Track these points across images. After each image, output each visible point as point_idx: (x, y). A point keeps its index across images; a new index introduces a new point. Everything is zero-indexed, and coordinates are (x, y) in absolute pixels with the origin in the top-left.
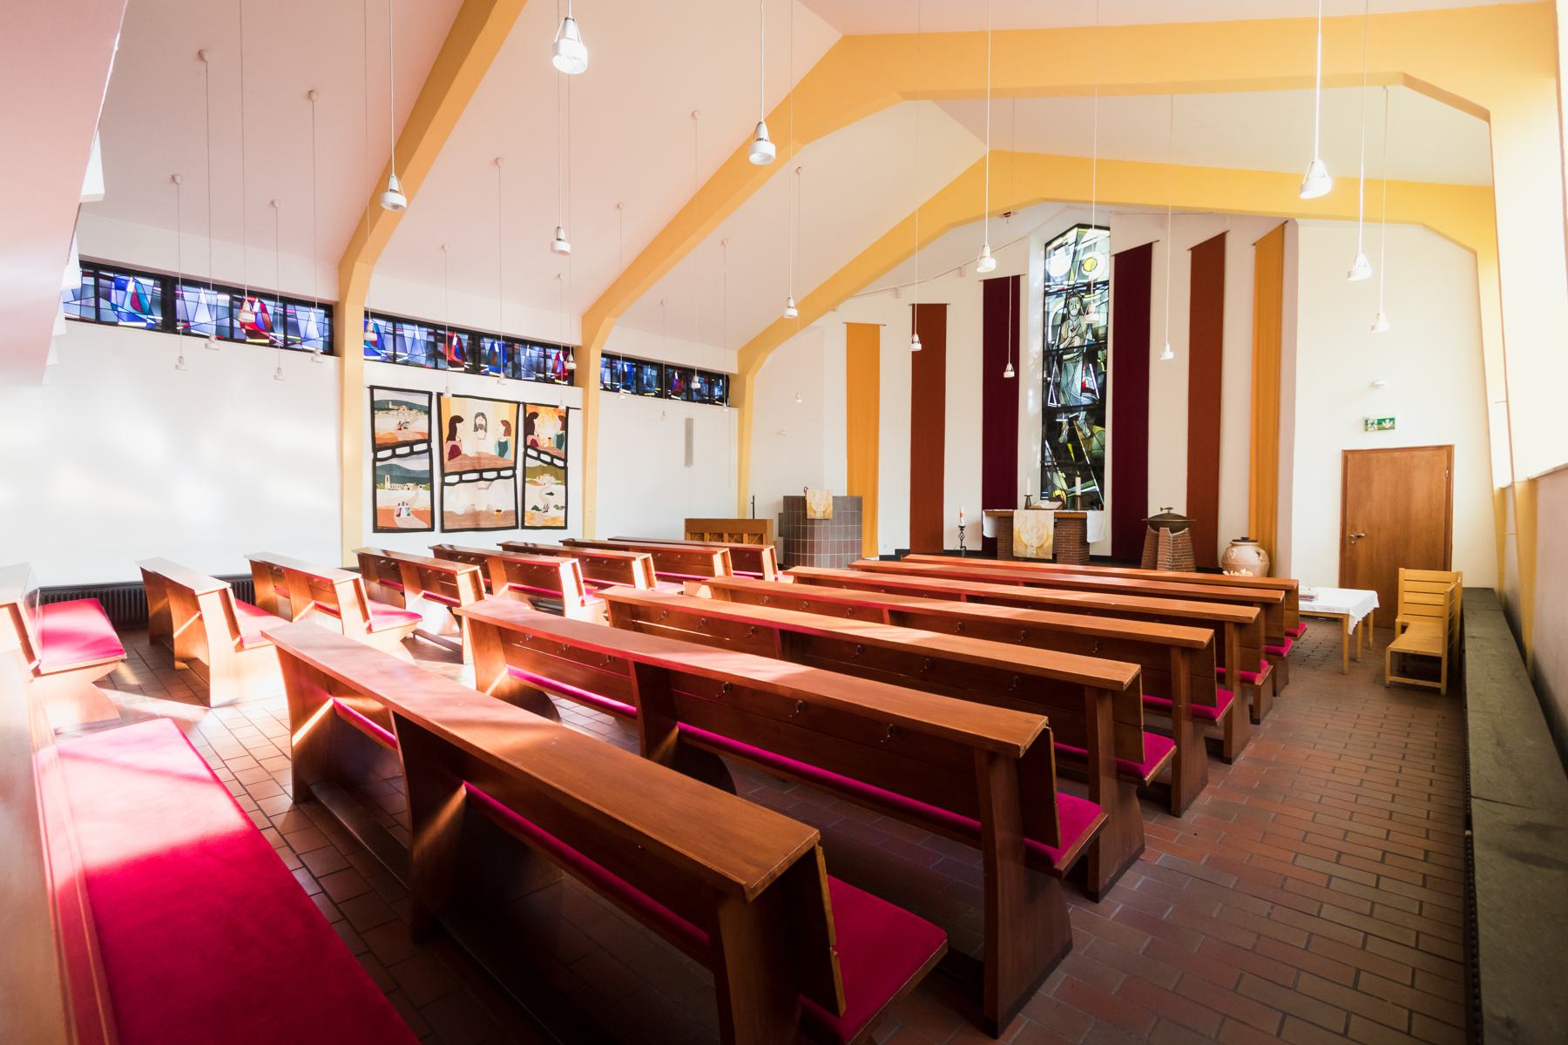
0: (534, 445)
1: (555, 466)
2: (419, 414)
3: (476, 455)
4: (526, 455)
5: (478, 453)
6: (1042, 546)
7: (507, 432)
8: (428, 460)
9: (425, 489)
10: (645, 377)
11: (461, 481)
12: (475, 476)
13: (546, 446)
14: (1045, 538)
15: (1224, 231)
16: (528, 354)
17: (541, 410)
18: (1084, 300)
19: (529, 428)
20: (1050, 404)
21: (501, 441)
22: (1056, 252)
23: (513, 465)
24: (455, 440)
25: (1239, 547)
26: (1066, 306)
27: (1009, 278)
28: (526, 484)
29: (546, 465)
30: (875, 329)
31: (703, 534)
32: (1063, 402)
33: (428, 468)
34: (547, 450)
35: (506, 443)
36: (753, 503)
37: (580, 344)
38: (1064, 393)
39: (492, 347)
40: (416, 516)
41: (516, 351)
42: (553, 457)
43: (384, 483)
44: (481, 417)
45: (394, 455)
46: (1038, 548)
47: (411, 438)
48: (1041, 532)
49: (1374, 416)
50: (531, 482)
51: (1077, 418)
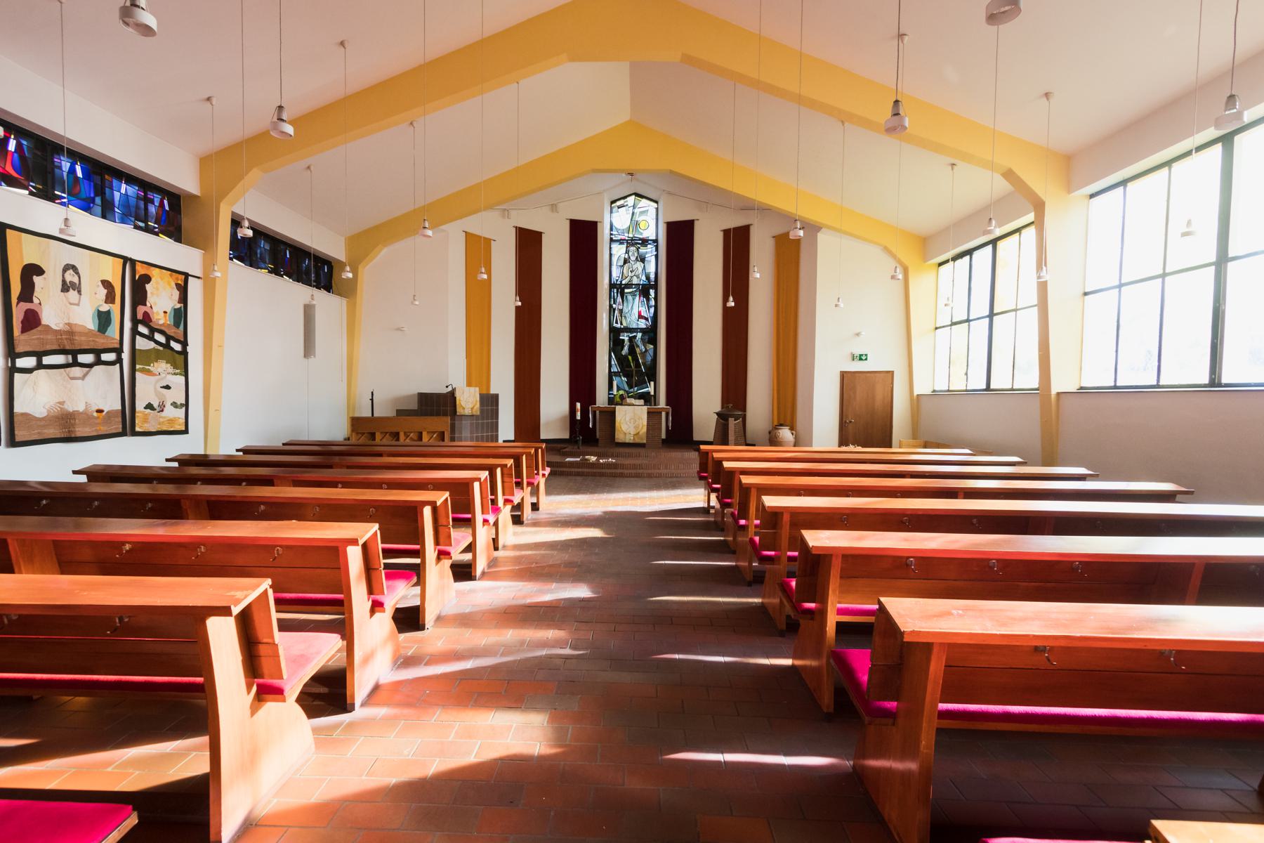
0: (147, 320)
1: (172, 349)
3: (67, 328)
4: (135, 332)
5: (69, 324)
7: (110, 298)
10: (259, 251)
11: (40, 366)
12: (59, 359)
13: (161, 322)
14: (640, 427)
15: (750, 223)
16: (123, 191)
17: (155, 273)
18: (640, 250)
19: (139, 295)
20: (615, 325)
21: (176, 307)
22: (620, 209)
23: (117, 346)
26: (627, 252)
28: (137, 373)
29: (161, 348)
30: (488, 242)
32: (625, 324)
34: (163, 328)
35: (108, 312)
36: (372, 400)
37: (199, 194)
39: (72, 171)
41: (107, 183)
42: (169, 338)
44: (71, 271)
49: (857, 352)
50: (142, 371)
51: (635, 337)
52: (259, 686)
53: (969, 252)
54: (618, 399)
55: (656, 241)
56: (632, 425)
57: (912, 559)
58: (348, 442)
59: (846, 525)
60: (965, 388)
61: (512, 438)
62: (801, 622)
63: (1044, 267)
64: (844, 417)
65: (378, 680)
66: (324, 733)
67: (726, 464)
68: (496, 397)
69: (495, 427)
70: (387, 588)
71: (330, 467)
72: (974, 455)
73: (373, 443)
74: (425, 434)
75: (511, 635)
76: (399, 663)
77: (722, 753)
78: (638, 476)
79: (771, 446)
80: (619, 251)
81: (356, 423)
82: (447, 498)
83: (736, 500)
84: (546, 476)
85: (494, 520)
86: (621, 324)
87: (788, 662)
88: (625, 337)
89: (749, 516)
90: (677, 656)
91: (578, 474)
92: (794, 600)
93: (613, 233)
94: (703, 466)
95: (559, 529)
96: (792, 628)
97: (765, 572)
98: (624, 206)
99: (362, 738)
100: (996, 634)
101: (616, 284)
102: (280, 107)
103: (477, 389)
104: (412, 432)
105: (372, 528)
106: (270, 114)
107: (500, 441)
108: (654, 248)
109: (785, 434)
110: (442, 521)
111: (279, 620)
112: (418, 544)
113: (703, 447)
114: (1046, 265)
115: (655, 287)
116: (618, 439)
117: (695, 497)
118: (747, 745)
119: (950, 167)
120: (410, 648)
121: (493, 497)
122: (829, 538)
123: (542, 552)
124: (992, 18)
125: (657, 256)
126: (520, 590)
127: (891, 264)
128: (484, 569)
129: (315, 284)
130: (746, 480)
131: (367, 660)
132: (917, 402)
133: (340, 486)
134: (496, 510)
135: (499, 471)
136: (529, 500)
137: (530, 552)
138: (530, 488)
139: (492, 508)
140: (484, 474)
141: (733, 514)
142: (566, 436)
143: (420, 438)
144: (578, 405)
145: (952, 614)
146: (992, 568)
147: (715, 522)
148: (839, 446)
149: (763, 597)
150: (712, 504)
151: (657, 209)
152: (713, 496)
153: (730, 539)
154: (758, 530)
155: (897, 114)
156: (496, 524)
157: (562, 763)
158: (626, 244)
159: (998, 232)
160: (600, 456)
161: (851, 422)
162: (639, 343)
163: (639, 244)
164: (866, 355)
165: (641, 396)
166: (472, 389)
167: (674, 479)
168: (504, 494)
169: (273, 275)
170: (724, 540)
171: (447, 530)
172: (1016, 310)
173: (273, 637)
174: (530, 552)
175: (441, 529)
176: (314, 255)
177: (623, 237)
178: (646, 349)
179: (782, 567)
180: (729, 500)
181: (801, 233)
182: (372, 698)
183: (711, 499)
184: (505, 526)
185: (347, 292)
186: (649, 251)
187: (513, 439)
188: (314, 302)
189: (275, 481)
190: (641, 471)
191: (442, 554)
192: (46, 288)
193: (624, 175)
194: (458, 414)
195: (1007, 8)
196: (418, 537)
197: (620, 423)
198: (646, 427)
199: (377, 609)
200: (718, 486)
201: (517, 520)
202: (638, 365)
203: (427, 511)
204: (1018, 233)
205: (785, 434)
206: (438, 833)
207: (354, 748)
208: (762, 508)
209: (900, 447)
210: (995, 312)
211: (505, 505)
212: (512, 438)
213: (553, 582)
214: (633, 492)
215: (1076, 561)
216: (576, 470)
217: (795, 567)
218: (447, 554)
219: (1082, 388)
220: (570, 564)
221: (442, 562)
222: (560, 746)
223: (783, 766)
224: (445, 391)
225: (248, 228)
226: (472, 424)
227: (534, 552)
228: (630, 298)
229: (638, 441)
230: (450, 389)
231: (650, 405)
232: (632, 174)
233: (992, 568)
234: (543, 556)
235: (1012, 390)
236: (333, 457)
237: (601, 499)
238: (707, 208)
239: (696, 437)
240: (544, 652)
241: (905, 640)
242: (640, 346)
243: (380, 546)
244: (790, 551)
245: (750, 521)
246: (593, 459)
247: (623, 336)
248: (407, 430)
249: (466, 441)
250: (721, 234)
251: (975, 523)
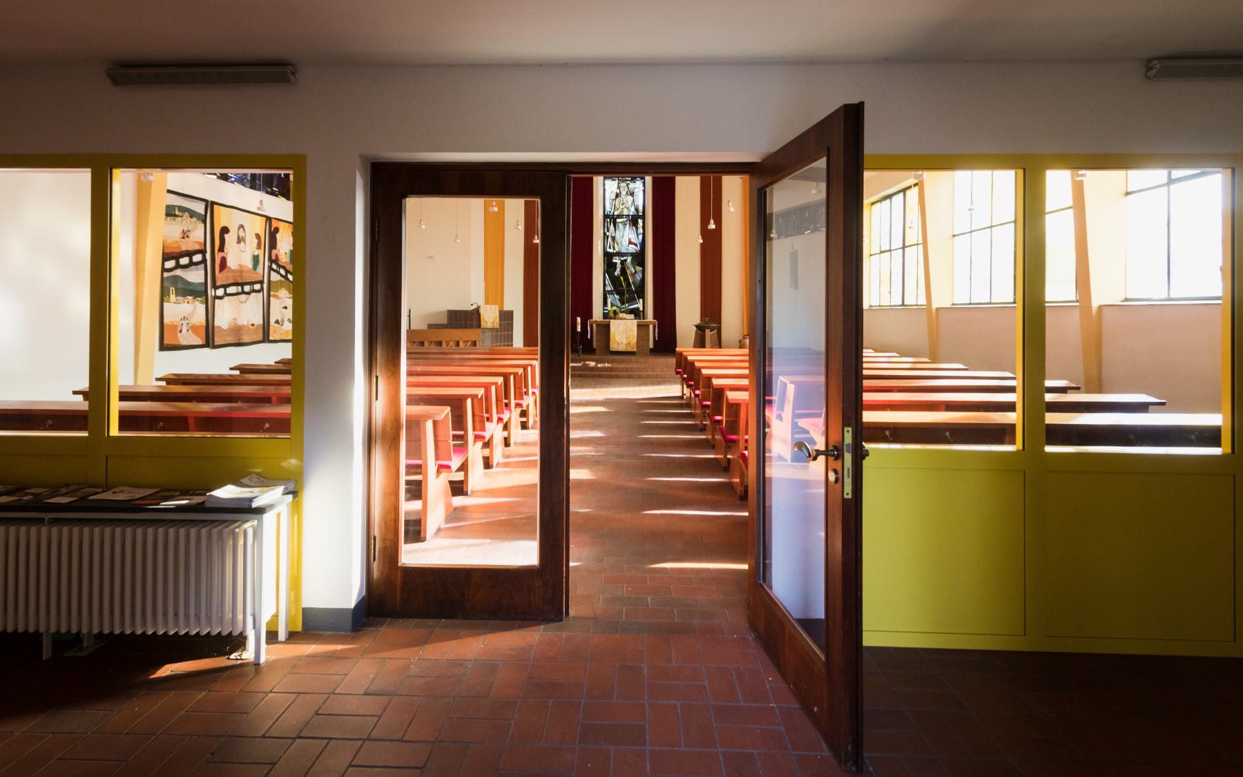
1: (288, 279)
2: (197, 222)
4: (270, 269)
5: (240, 266)
6: (629, 343)
7: (259, 247)
8: (203, 272)
9: (201, 302)
11: (226, 294)
13: (284, 261)
20: (608, 250)
24: (224, 251)
26: (619, 188)
28: (271, 298)
31: (423, 342)
33: (203, 281)
34: (284, 265)
35: (258, 256)
36: (409, 316)
38: (617, 243)
40: (193, 332)
42: (287, 272)
43: (169, 295)
45: (178, 266)
46: (626, 344)
47: (191, 247)
48: (628, 334)
51: (626, 260)
53: (889, 197)
69: (510, 338)
72: (932, 363)
74: (461, 343)
78: (629, 377)
86: (614, 249)
88: (617, 260)
89: (739, 432)
90: (653, 455)
94: (678, 365)
101: (610, 215)
103: (497, 307)
105: (446, 409)
108: (642, 184)
115: (643, 217)
117: (674, 390)
128: (440, 524)
140: (500, 380)
144: (579, 319)
160: (598, 361)
167: (660, 379)
168: (474, 429)
175: (441, 445)
190: (632, 373)
192: (230, 239)
201: (487, 464)
202: (629, 285)
203: (429, 425)
216: (579, 373)
223: (699, 482)
226: (492, 336)
228: (621, 226)
230: (474, 307)
231: (640, 319)
236: (281, 387)
240: (581, 454)
246: (592, 364)
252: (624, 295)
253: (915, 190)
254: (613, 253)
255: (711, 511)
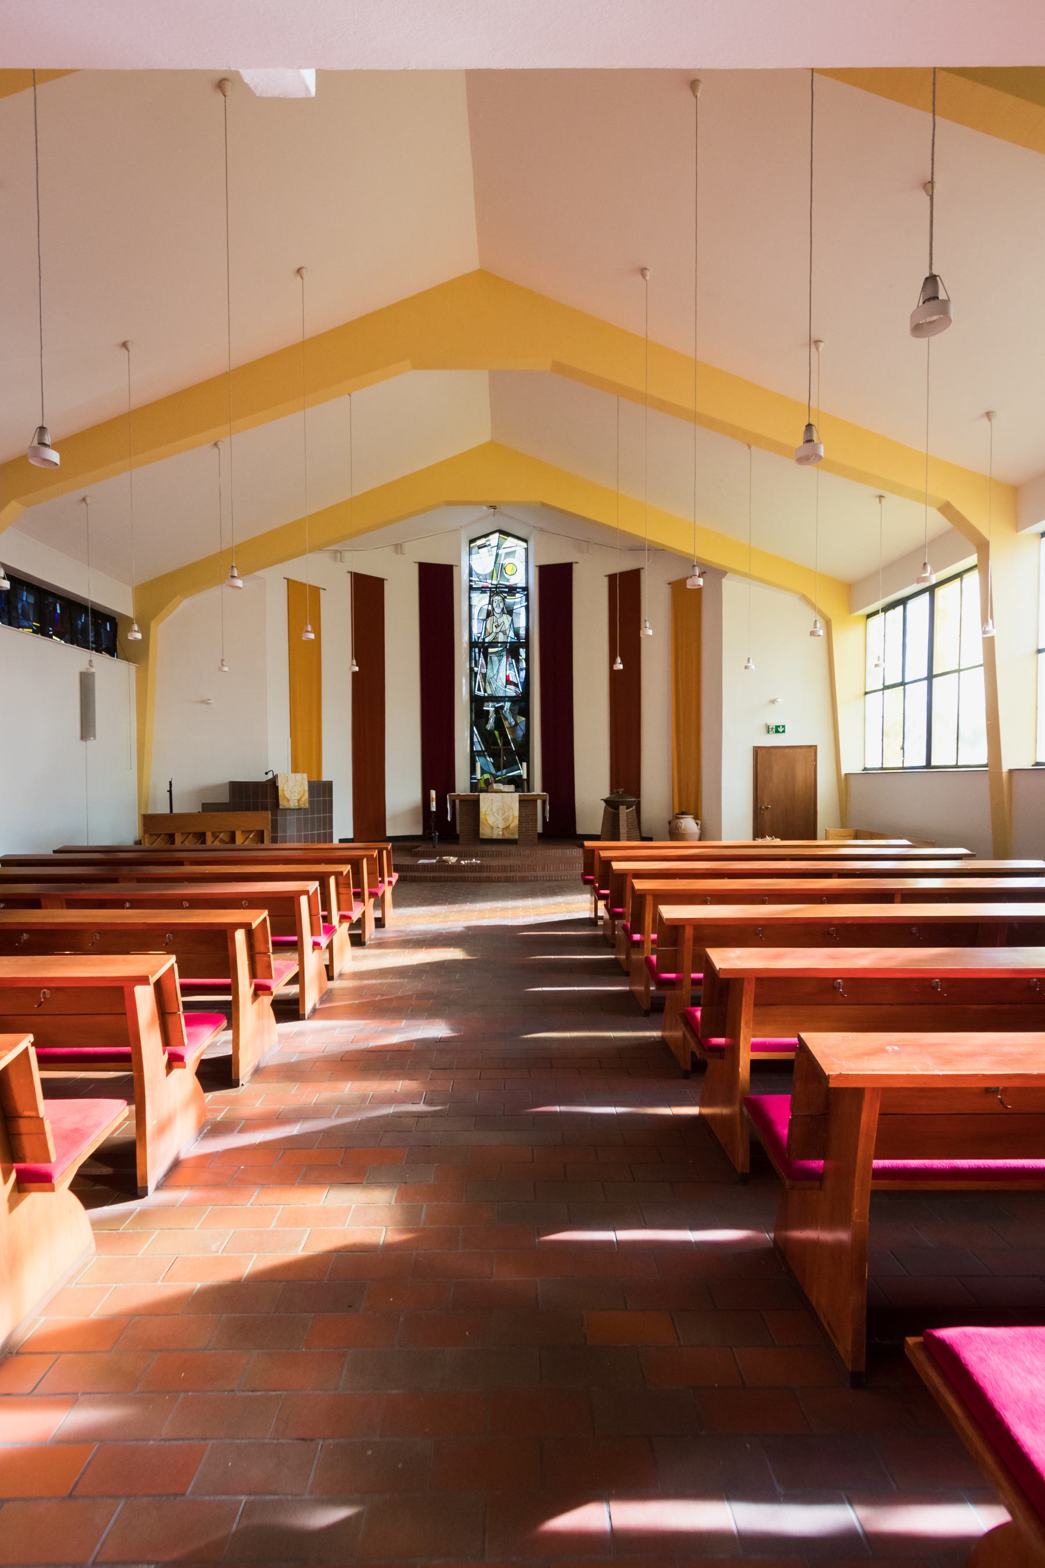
10: (20, 605)
14: (511, 820)
18: (506, 600)
20: (477, 693)
22: (480, 550)
25: (685, 819)
26: (491, 603)
27: (616, 574)
30: (316, 591)
36: (170, 791)
46: (503, 829)
49: (773, 723)
52: (19, 1172)
53: (903, 602)
54: (482, 785)
55: (526, 589)
56: (500, 817)
57: (840, 981)
58: (138, 847)
59: (761, 938)
60: (901, 766)
61: (351, 836)
62: (709, 1061)
63: (989, 619)
64: (759, 801)
65: (178, 1154)
66: (108, 1228)
67: (616, 866)
68: (329, 786)
69: (328, 822)
70: (189, 1035)
71: (115, 880)
73: (172, 847)
74: (238, 834)
75: (349, 1089)
76: (205, 1131)
77: (614, 1230)
78: (508, 880)
79: (672, 840)
80: (480, 601)
81: (150, 821)
82: (265, 918)
83: (628, 909)
84: (394, 883)
85: (327, 942)
86: (485, 691)
87: (694, 1111)
88: (490, 707)
89: (644, 931)
90: (557, 1109)
91: (434, 880)
92: (699, 1036)
93: (473, 579)
94: (588, 868)
95: (411, 950)
96: (699, 1067)
97: (664, 998)
98: (486, 546)
99: (158, 1231)
100: (939, 1075)
101: (478, 642)
102: (42, 429)
103: (305, 775)
104: (222, 832)
105: (168, 960)
106: (29, 439)
107: (336, 841)
108: (524, 598)
109: (689, 824)
110: (259, 947)
111: (44, 1081)
112: (229, 978)
113: (587, 843)
114: (992, 618)
115: (527, 645)
116: (483, 834)
118: (644, 1219)
119: (878, 500)
120: (220, 1111)
121: (325, 913)
122: (739, 958)
123: (389, 981)
124: (918, 329)
125: (527, 608)
126: (361, 1030)
127: (811, 615)
128: (315, 1005)
129: (94, 646)
130: (640, 885)
131: (162, 1128)
132: (845, 783)
133: (128, 905)
134: (330, 930)
135: (332, 880)
136: (372, 914)
137: (373, 982)
138: (372, 900)
139: (324, 927)
140: (313, 886)
141: (624, 927)
142: (418, 831)
143: (233, 840)
144: (433, 793)
145: (886, 1051)
146: (934, 988)
147: (604, 936)
148: (754, 839)
149: (663, 1029)
150: (600, 914)
151: (527, 550)
152: (601, 904)
153: (622, 957)
154: (655, 946)
155: (809, 441)
156: (330, 947)
157: (414, 1253)
158: (488, 592)
159: (934, 580)
160: (461, 856)
161: (767, 808)
162: (508, 715)
163: (505, 592)
164: (784, 726)
165: (510, 781)
166: (299, 776)
167: (554, 884)
168: (339, 909)
169: (39, 636)
170: (616, 959)
171: (266, 958)
172: (959, 671)
173: (36, 1109)
174: (373, 982)
175: (258, 957)
176: (91, 608)
177: (485, 584)
178: (516, 722)
179: (686, 992)
180: (621, 910)
181: (701, 582)
182: (167, 1182)
183: (599, 907)
184: (342, 949)
185: (137, 655)
186: (518, 601)
187: (351, 836)
188: (93, 670)
189: (42, 900)
190: (512, 874)
191: (260, 990)
193: (485, 508)
194: (281, 807)
195: (934, 318)
196: (229, 967)
197: (485, 814)
198: (518, 819)
199: (174, 1064)
200: (607, 892)
201: (357, 941)
202: (506, 742)
203: (240, 936)
204: (959, 579)
205: (689, 824)
206: (256, 1352)
207: (145, 1247)
208: (659, 922)
209: (826, 839)
210: (934, 673)
211: (340, 922)
212: (351, 836)
213: (403, 1019)
214: (502, 900)
215: (1033, 978)
216: (432, 874)
217: (700, 991)
218: (267, 989)
219: (1037, 764)
220: (423, 996)
221: (260, 998)
222: (410, 1231)
223: (688, 1243)
224: (264, 778)
225: (4, 578)
227: (379, 981)
228: (495, 658)
229: (507, 836)
230: (270, 776)
232: (494, 508)
233: (934, 988)
234: (391, 985)
235: (957, 766)
237: (463, 911)
238: (588, 547)
239: (580, 830)
240: (391, 1110)
241: (831, 1085)
242: (509, 718)
243: (178, 981)
244: (693, 972)
245: (646, 936)
246: (453, 860)
247: (488, 706)
248: (213, 830)
249: (292, 842)
250: (605, 582)
251: (914, 932)
252: (500, 755)
253: (975, 574)
254: (484, 697)
255: (594, 986)
